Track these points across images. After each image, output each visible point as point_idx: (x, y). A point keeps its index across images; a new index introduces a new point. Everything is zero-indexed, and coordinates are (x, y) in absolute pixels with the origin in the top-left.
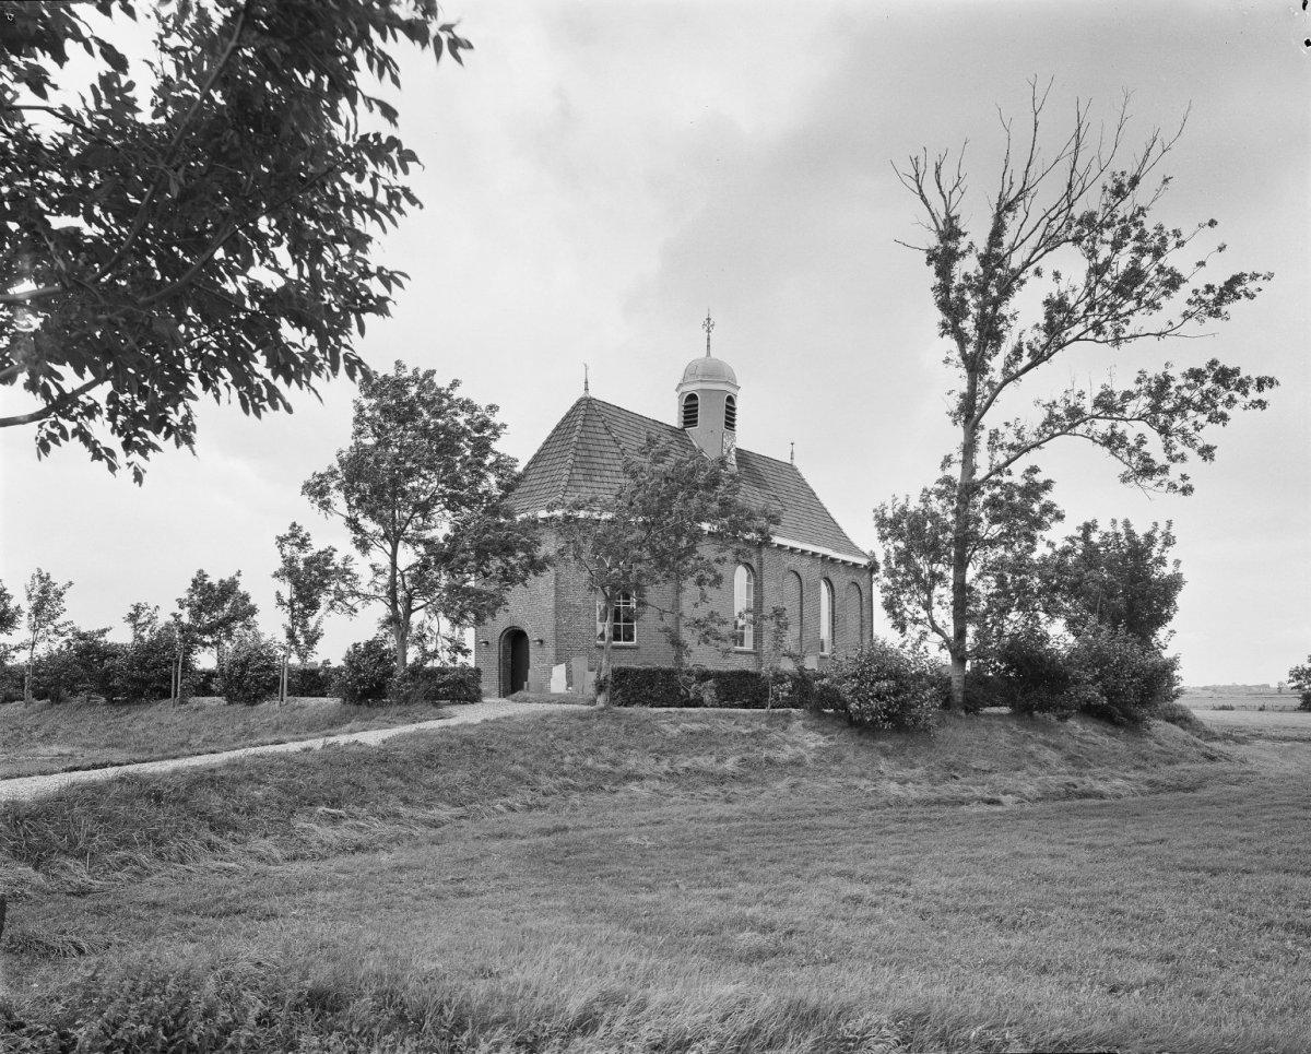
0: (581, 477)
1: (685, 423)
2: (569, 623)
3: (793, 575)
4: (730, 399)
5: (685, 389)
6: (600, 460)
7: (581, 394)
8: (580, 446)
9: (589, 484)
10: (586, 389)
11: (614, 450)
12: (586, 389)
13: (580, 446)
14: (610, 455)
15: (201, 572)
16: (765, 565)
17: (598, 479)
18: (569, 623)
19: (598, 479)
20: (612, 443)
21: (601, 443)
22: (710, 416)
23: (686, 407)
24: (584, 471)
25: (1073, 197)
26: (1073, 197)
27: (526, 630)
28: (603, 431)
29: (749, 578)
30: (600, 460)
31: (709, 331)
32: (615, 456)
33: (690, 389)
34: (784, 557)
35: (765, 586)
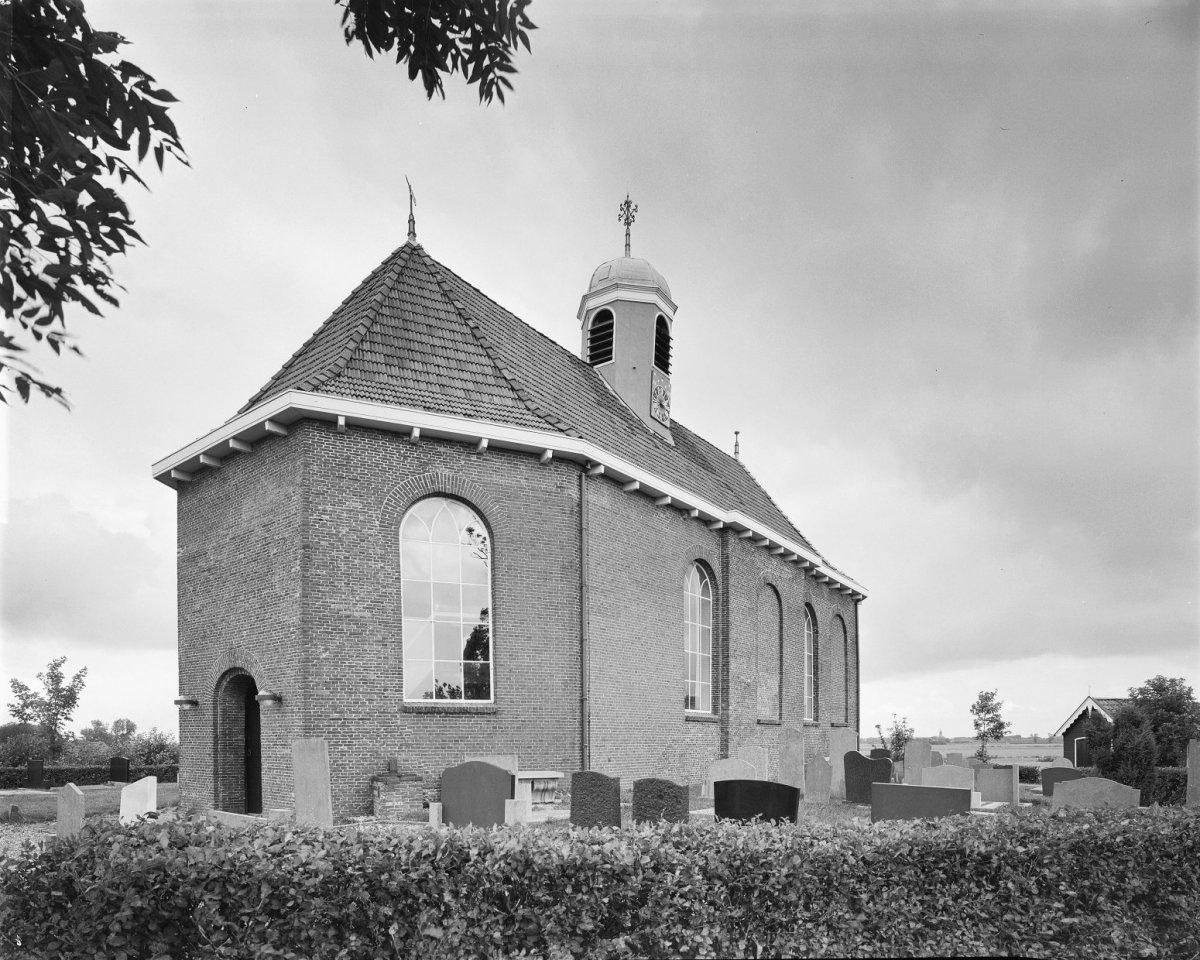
0: (380, 358)
1: (592, 357)
2: (338, 658)
3: (769, 591)
4: (662, 324)
5: (591, 304)
6: (424, 339)
7: (401, 240)
8: (385, 311)
9: (395, 371)
10: (412, 233)
11: (456, 327)
12: (412, 233)
13: (385, 311)
14: (447, 335)
15: (9, 705)
16: (732, 567)
17: (418, 366)
18: (338, 658)
19: (418, 366)
20: (454, 317)
21: (431, 313)
22: (631, 345)
23: (592, 340)
24: (388, 351)
25: (752, 625)
26: (752, 625)
27: (253, 672)
28: (438, 297)
29: (702, 577)
30: (424, 339)
31: (628, 224)
32: (458, 337)
33: (597, 303)
34: (760, 558)
35: (733, 605)
